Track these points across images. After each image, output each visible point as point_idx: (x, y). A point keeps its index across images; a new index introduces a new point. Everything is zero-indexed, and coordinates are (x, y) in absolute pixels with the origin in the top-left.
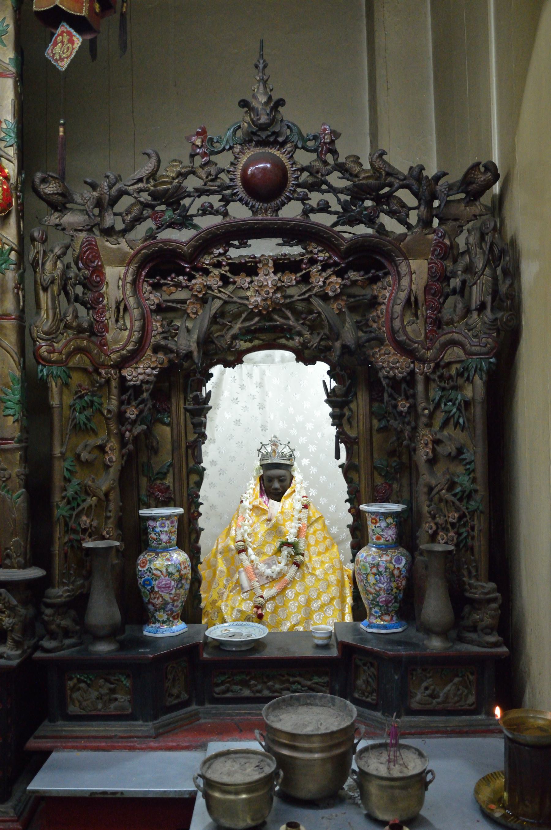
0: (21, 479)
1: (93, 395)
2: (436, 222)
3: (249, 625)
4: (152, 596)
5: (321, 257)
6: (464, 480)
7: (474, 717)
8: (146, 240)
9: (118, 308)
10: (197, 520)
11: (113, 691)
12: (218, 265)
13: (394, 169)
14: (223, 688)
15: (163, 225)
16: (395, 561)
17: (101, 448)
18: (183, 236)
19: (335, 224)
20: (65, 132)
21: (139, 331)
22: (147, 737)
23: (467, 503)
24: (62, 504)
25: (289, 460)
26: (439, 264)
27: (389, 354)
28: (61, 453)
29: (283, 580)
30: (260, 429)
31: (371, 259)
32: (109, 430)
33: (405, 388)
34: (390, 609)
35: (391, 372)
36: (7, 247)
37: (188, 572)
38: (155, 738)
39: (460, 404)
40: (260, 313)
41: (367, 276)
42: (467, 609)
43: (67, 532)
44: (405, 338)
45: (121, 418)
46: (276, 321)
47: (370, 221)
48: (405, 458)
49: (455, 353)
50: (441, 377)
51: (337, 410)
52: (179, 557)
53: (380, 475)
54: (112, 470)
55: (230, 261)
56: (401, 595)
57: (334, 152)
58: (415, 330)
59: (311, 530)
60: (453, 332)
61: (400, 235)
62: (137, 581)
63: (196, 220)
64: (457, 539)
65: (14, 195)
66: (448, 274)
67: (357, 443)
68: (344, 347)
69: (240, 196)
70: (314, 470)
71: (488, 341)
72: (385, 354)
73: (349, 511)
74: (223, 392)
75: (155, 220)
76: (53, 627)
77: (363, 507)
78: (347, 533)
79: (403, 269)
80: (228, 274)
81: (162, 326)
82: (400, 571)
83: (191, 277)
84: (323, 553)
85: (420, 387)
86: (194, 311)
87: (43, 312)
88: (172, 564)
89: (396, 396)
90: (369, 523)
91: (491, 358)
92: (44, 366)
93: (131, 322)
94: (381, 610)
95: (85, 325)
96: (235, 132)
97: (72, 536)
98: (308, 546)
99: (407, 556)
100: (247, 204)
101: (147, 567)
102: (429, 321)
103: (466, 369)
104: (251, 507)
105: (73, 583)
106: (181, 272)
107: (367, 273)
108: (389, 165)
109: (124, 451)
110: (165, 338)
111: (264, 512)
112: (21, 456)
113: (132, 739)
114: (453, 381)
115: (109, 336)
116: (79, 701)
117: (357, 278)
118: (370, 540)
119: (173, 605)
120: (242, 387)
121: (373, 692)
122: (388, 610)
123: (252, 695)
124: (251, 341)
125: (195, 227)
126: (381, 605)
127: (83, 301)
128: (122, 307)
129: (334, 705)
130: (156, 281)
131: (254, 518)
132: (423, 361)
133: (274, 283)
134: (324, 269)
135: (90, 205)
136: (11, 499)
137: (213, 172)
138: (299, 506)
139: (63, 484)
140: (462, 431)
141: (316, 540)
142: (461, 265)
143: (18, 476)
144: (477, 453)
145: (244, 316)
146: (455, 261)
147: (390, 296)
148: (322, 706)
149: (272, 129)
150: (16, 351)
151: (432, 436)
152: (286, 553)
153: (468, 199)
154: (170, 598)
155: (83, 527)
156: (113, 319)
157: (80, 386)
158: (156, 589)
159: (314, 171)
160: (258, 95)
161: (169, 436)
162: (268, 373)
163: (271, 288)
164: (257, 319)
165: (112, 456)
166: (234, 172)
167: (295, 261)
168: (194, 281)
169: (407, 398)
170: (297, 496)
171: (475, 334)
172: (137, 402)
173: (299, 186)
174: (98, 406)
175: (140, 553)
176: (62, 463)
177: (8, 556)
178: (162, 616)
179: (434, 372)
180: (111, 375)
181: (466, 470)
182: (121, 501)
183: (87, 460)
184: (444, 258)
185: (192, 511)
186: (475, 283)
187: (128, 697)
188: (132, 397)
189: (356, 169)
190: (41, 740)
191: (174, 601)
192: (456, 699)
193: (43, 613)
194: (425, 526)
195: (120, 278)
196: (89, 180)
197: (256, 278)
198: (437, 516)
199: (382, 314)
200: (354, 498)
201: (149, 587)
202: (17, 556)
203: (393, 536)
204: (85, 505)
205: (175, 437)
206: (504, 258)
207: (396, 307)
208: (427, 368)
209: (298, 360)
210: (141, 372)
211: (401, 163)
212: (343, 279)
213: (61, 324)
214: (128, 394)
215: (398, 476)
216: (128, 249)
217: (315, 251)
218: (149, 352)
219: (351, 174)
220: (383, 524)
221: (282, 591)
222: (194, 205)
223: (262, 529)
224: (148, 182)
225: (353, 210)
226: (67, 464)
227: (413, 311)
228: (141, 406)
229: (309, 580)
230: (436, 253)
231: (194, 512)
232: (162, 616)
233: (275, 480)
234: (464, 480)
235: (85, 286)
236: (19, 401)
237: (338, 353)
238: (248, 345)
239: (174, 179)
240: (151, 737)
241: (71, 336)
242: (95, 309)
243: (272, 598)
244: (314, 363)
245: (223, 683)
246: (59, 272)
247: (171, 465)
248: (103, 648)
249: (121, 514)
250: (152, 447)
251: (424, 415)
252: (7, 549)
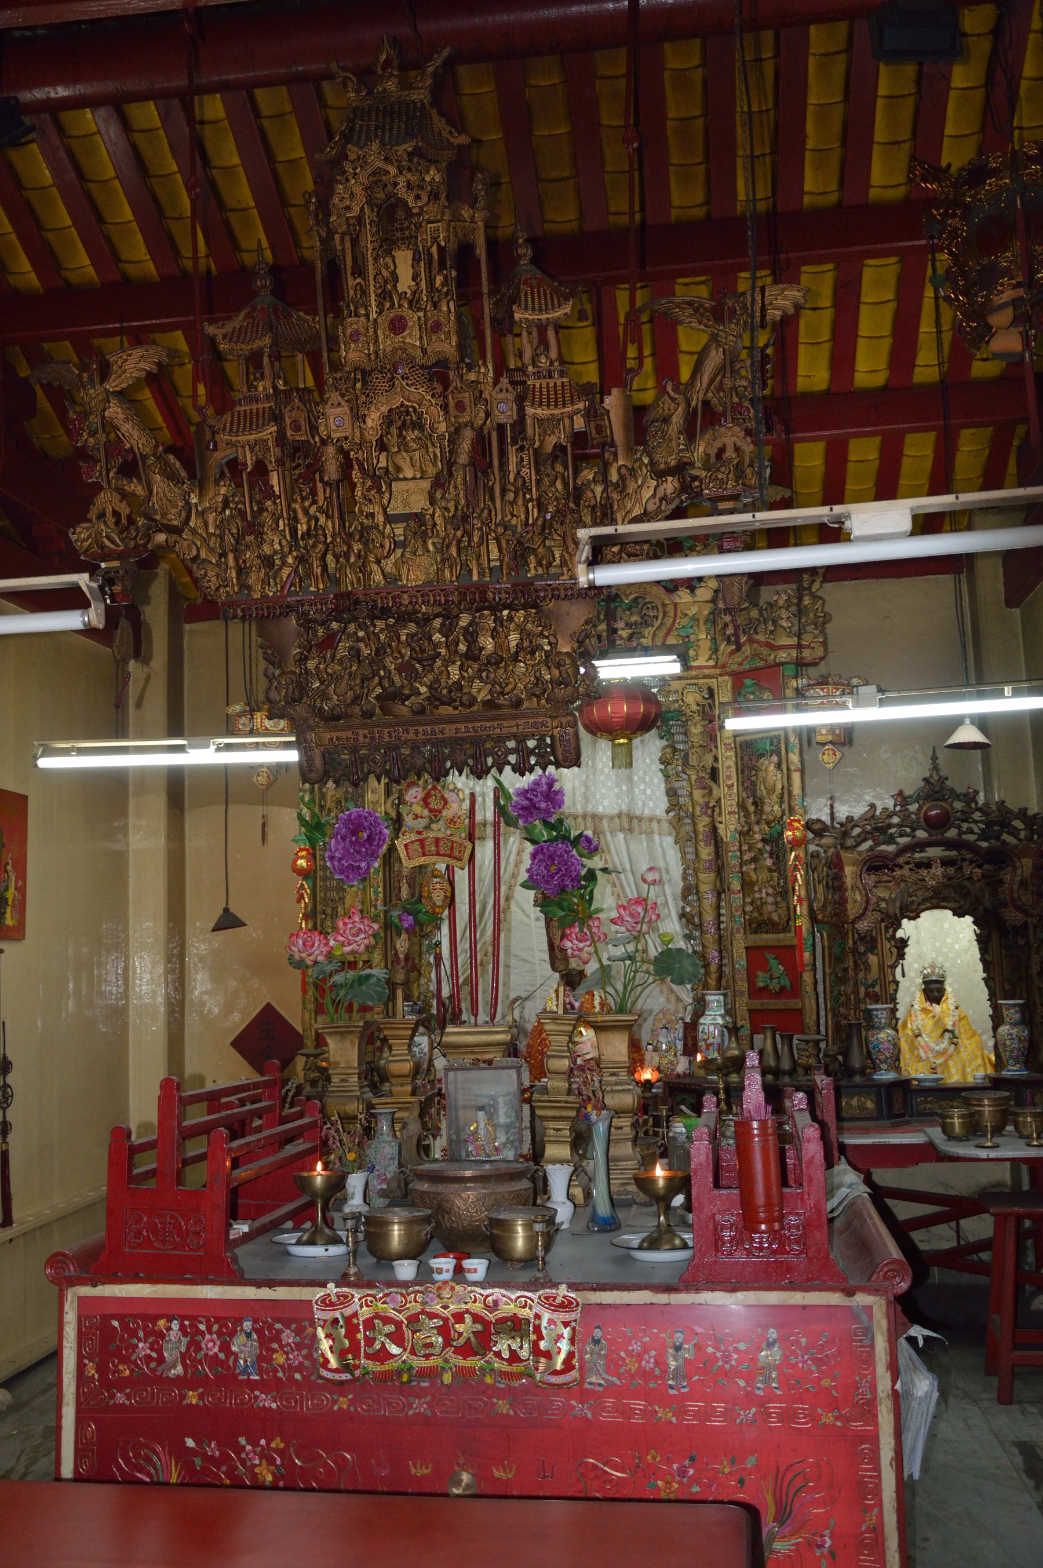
12: (908, 863)
31: (1000, 857)
68: (986, 910)
79: (1018, 864)
85: (1031, 931)
125: (896, 843)
132: (1032, 916)
138: (952, 1007)
200: (993, 997)
211: (1013, 805)
223: (930, 1023)
233: (934, 990)
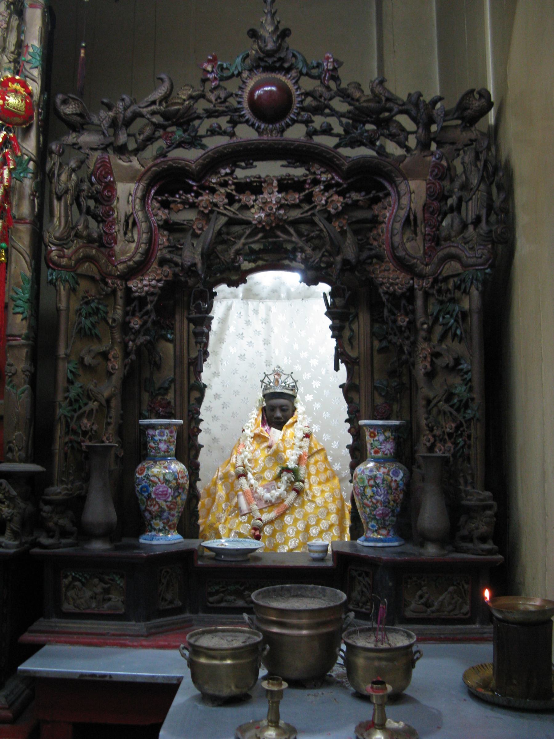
0: (27, 376)
1: (99, 303)
2: (434, 146)
3: (245, 542)
4: (149, 503)
5: (324, 178)
6: (461, 390)
7: (469, 626)
8: (156, 158)
10: (197, 436)
11: (107, 591)
12: (224, 184)
13: (392, 95)
14: (216, 598)
15: (173, 144)
16: (393, 474)
17: (105, 355)
18: (191, 156)
19: (337, 146)
20: (85, 54)
21: (146, 244)
22: (139, 636)
23: (465, 412)
24: (65, 404)
25: (292, 390)
26: (437, 184)
27: (389, 270)
28: (66, 354)
29: (281, 505)
30: (264, 364)
31: (371, 180)
32: (113, 338)
33: (404, 305)
34: (387, 523)
35: (391, 288)
36: (26, 157)
37: (185, 481)
38: (147, 636)
39: (457, 315)
40: (263, 229)
41: (367, 197)
42: (463, 519)
43: (67, 433)
44: (404, 253)
45: (125, 327)
46: (279, 237)
47: (371, 143)
48: (405, 379)
49: (453, 267)
50: (439, 291)
51: (337, 321)
52: (177, 467)
53: (380, 394)
54: (114, 377)
55: (235, 181)
56: (398, 509)
57: (335, 78)
58: (414, 247)
59: (312, 460)
60: (450, 246)
61: (400, 156)
62: (135, 488)
63: (205, 141)
64: (454, 449)
65: (36, 111)
66: (446, 193)
67: (358, 364)
68: (346, 262)
69: (247, 117)
70: (317, 406)
71: (483, 252)
72: (385, 270)
73: (349, 431)
74: (229, 327)
75: (166, 139)
76: (51, 524)
77: (361, 422)
78: (346, 452)
79: (403, 188)
80: (234, 193)
81: (168, 240)
82: (398, 484)
83: (198, 195)
84: (324, 483)
85: (419, 302)
86: (200, 226)
87: (56, 219)
88: (170, 473)
89: (396, 312)
90: (368, 437)
91: (487, 269)
92: (54, 270)
93: (139, 234)
94: (377, 524)
95: (95, 235)
96: (244, 59)
97: (73, 437)
98: (309, 475)
99: (405, 470)
100: (253, 125)
101: (145, 474)
102: (428, 238)
103: (463, 281)
104: (252, 435)
105: (72, 482)
106: (188, 190)
107: (368, 193)
108: (389, 92)
109: (126, 361)
110: (170, 252)
111: (265, 439)
112: (27, 352)
113: (124, 637)
114: (450, 293)
115: (117, 248)
116: (73, 599)
117: (358, 198)
118: (368, 455)
119: (169, 514)
120: (248, 323)
121: (367, 602)
122: (385, 524)
123: (246, 605)
124: (254, 261)
125: (203, 147)
126: (378, 518)
127: (94, 214)
128: (130, 222)
129: (324, 596)
130: (164, 198)
131: (255, 445)
132: (421, 276)
133: (278, 200)
134: (326, 189)
135: (105, 124)
136: (16, 394)
137: (223, 96)
138: (300, 435)
139: (66, 385)
140: (460, 342)
141: (317, 471)
142: (457, 184)
143: (23, 372)
144: (473, 364)
146: (452, 181)
147: (391, 215)
148: (311, 597)
149: (278, 55)
150: (28, 252)
151: (431, 349)
152: (286, 478)
154: (167, 506)
155: (84, 429)
156: (122, 232)
157: (87, 292)
158: (153, 496)
159: (317, 95)
160: (266, 25)
161: (172, 352)
162: (274, 309)
163: (274, 205)
164: (260, 235)
165: (114, 363)
166: (241, 95)
167: (299, 181)
168: (200, 198)
169: (407, 314)
170: (298, 425)
171: (471, 247)
172: (142, 313)
173: (303, 109)
174: (103, 315)
175: (140, 462)
176: (66, 365)
177: (11, 450)
178: (158, 524)
179: (432, 287)
180: (118, 285)
181: (464, 380)
182: (122, 410)
183: (90, 365)
184: (441, 179)
185: (192, 427)
186: (471, 199)
187: (122, 598)
188: (137, 309)
189: (357, 94)
190: (34, 634)
191: (170, 509)
192: (451, 607)
193: (41, 510)
194: (423, 439)
195: (130, 194)
196: (105, 101)
197: (261, 196)
198: (435, 428)
199: (382, 232)
201: (146, 494)
202: (19, 450)
203: (392, 450)
204: (87, 409)
205: (178, 353)
206: (498, 177)
207: (395, 224)
208: (425, 284)
210: (145, 284)
211: (401, 90)
212: (344, 198)
213: (71, 234)
214: (133, 305)
215: (398, 396)
216: (138, 166)
217: (319, 172)
218: (155, 265)
219: (353, 99)
220: (382, 438)
221: (281, 516)
222: (203, 126)
226: (71, 367)
227: (412, 228)
228: (145, 317)
229: (309, 508)
230: (434, 173)
231: (194, 427)
232: (158, 524)
233: (277, 408)
234: (461, 390)
235: (97, 201)
236: (28, 300)
237: (339, 266)
238: (252, 265)
239: (184, 100)
240: (142, 636)
241: (81, 244)
242: (105, 221)
243: (271, 522)
245: (217, 592)
246: (73, 183)
247: (173, 381)
248: (98, 546)
249: (121, 421)
250: (155, 363)
251: (423, 330)
252: (10, 442)
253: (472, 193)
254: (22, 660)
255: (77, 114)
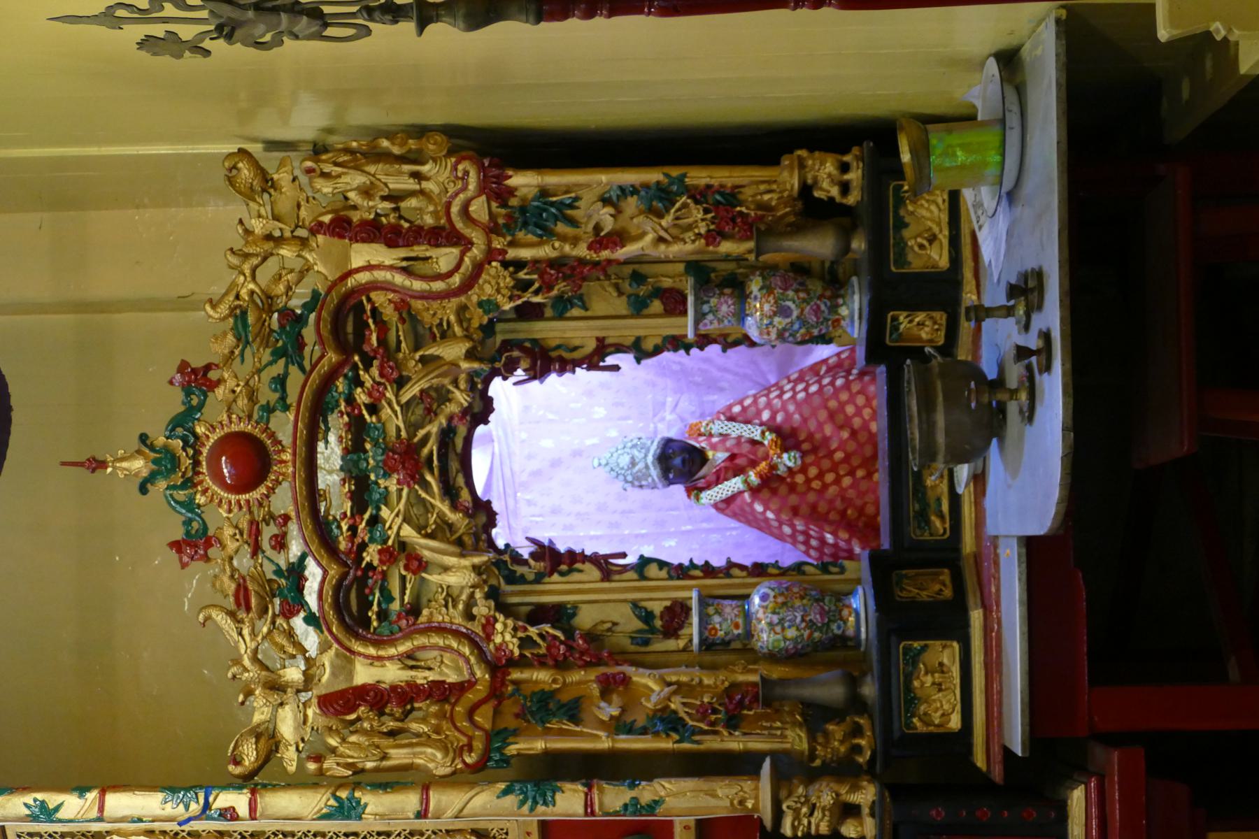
9: (412, 668)
34: (833, 608)
67: (604, 338)
76: (843, 749)
94: (835, 621)
100: (272, 490)
110: (454, 606)
125: (303, 558)
130: (374, 617)
145: (424, 495)
153: (272, 191)
156: (427, 673)
186: (386, 184)
192: (933, 208)
209: (486, 422)
216: (332, 652)
220: (717, 619)
224: (241, 621)
225: (285, 344)
244: (491, 400)
253: (378, 183)
254: (1015, 755)
255: (256, 743)
